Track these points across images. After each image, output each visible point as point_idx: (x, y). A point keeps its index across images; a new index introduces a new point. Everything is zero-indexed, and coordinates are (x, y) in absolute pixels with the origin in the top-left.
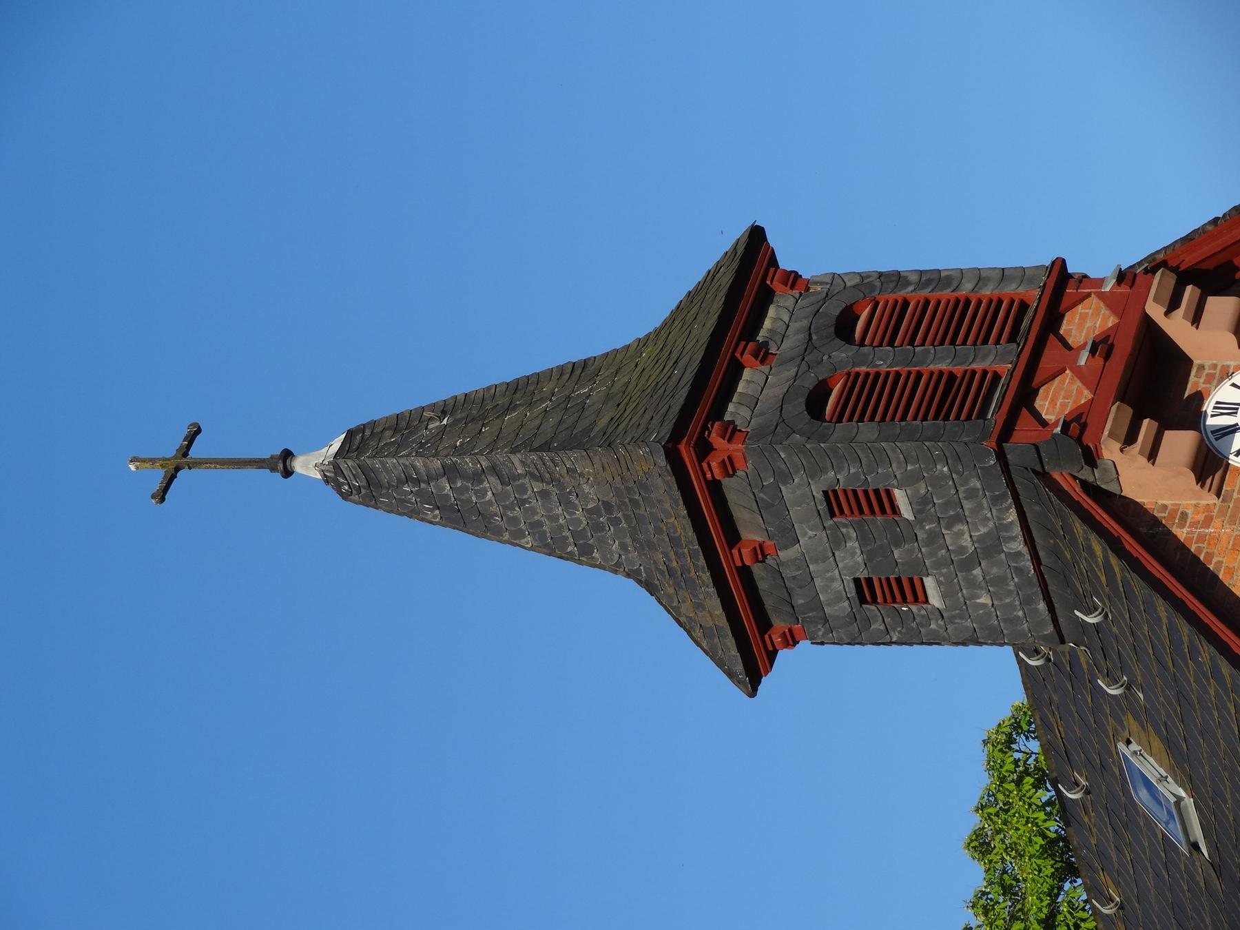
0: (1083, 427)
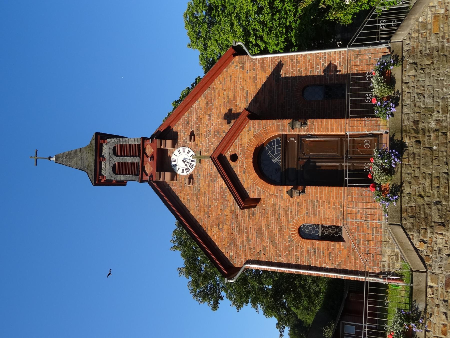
0: (152, 177)
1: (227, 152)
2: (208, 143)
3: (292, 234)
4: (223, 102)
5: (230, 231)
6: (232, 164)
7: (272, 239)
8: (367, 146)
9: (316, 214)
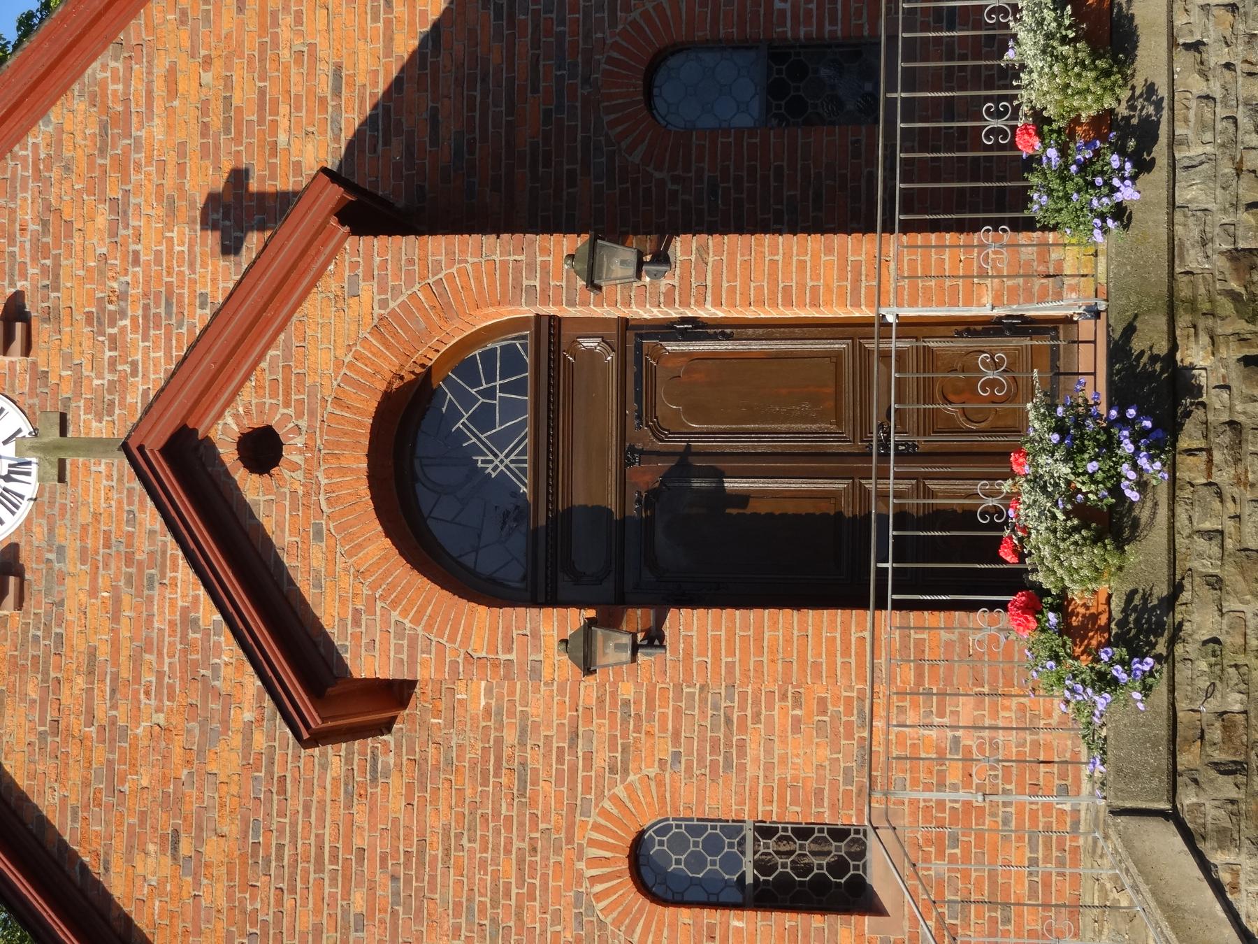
1: (220, 415)
2: (113, 363)
3: (594, 880)
4: (196, 129)
5: (243, 875)
6: (251, 487)
7: (482, 911)
8: (992, 383)
9: (728, 764)
